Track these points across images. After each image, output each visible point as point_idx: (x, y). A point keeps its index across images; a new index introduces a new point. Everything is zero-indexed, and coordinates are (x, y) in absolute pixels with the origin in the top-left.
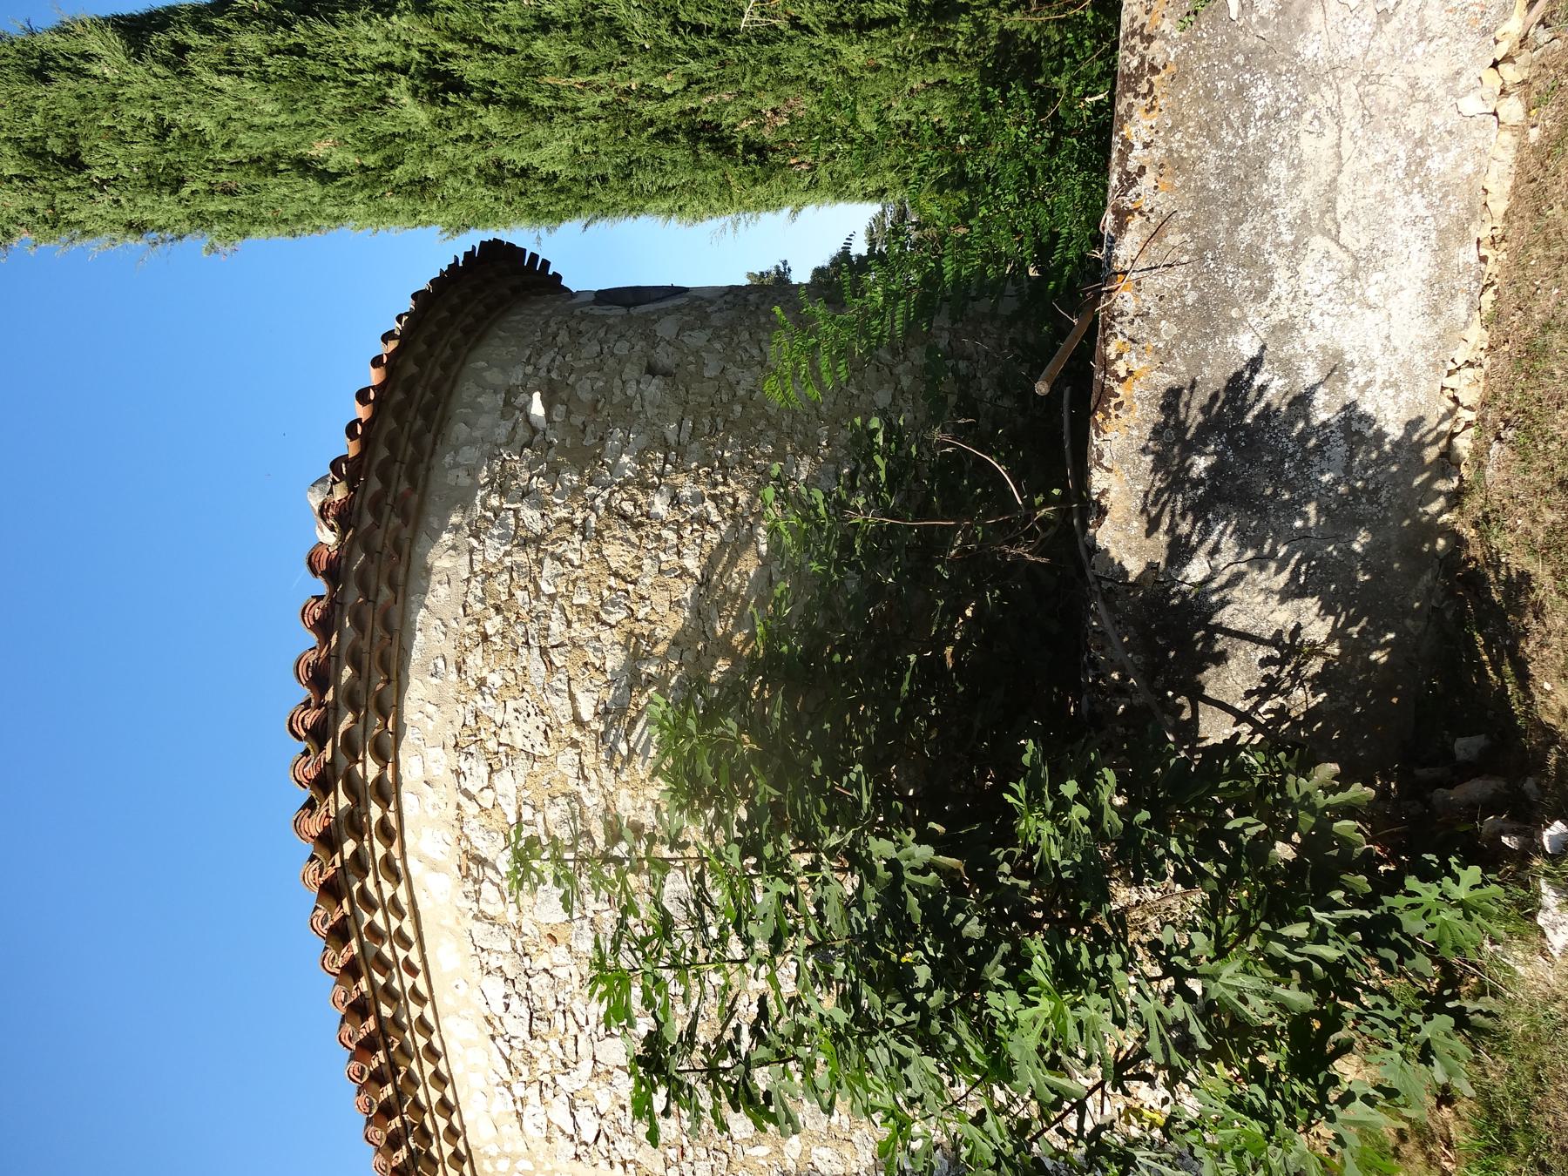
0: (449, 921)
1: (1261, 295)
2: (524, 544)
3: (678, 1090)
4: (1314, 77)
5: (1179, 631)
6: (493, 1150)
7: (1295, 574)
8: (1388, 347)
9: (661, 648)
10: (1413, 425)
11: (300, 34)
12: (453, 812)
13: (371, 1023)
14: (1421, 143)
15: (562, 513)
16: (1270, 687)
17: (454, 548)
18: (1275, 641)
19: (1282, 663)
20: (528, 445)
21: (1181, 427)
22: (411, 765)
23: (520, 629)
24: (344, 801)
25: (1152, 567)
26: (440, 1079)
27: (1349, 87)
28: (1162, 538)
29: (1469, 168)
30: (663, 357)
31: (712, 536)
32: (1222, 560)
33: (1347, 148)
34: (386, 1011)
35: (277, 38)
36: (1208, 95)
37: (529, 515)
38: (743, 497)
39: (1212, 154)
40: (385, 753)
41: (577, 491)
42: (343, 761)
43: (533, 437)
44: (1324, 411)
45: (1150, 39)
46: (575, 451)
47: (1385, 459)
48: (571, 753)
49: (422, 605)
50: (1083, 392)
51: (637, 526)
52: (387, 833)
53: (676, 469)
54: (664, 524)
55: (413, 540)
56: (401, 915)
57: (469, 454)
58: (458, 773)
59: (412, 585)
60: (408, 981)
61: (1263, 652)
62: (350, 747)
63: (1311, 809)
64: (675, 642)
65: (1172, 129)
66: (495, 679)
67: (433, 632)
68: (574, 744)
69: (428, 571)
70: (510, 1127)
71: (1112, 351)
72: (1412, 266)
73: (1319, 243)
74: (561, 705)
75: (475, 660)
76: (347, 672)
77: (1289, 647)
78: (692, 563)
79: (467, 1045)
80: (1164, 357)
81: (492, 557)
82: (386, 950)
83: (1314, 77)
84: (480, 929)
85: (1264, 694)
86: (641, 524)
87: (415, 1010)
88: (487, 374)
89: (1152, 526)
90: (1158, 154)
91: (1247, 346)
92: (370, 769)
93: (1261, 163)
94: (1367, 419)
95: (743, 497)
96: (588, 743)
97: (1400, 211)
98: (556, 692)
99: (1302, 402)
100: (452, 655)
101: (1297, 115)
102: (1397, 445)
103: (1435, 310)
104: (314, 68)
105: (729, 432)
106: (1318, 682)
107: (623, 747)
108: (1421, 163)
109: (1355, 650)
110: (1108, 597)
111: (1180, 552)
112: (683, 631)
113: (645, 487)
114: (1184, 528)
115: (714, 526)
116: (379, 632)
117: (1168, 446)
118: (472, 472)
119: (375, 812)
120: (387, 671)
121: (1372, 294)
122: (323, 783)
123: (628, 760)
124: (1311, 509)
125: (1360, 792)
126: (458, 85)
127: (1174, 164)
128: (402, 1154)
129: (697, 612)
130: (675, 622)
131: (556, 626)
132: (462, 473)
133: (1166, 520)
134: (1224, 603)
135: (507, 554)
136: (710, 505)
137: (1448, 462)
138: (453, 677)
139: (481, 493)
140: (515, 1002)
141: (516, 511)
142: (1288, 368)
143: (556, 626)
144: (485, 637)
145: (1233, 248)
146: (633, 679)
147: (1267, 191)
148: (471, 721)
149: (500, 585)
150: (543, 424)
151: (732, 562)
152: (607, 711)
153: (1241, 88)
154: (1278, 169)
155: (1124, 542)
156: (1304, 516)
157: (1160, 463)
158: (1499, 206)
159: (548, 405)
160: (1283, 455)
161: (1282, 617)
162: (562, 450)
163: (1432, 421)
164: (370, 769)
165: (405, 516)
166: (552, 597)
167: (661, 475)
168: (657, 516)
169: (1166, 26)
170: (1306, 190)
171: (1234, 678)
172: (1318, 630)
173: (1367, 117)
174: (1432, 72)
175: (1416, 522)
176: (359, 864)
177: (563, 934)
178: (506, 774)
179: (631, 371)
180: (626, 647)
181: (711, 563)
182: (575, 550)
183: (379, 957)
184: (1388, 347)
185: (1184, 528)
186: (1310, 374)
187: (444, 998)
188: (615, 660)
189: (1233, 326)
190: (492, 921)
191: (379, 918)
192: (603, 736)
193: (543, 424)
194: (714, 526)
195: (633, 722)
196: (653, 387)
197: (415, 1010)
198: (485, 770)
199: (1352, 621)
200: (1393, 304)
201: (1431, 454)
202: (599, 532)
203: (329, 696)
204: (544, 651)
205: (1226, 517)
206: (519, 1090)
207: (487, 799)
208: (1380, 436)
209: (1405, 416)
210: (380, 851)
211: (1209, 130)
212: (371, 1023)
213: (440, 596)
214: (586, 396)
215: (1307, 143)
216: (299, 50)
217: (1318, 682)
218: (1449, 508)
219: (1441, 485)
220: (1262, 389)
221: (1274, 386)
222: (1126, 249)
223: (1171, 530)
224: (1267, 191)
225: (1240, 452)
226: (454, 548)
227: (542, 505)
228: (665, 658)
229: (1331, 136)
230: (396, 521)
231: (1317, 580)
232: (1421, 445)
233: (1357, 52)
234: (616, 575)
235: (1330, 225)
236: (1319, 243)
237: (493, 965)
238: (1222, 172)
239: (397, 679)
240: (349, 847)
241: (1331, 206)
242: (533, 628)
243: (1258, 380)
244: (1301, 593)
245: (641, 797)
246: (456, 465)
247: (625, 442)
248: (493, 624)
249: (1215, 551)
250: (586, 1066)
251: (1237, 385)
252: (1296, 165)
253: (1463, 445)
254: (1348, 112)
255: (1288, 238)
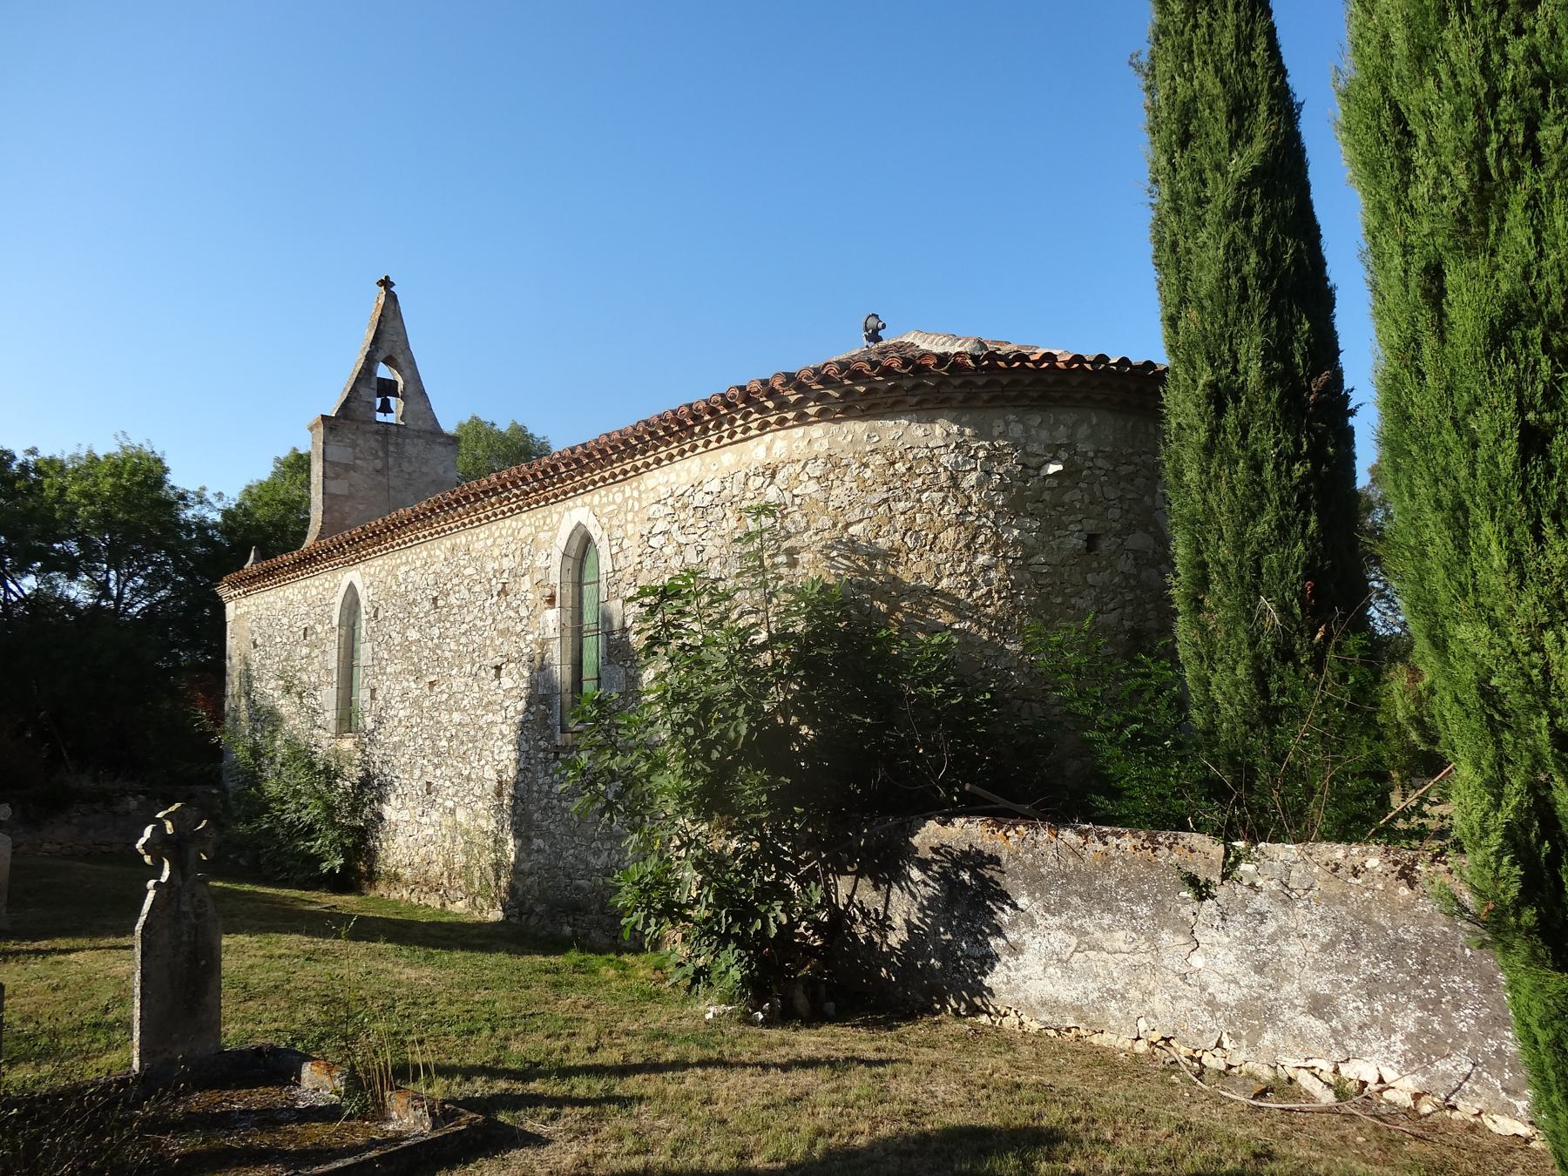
0: (744, 459)
1: (1047, 910)
2: (953, 478)
3: (652, 610)
4: (1152, 939)
5: (886, 864)
6: (642, 488)
7: (918, 928)
8: (1026, 978)
9: (891, 570)
10: (990, 991)
11: (1256, 296)
12: (796, 457)
13: (690, 423)
14: (1123, 997)
15: (975, 499)
16: (866, 915)
17: (948, 434)
18: (887, 918)
19: (876, 920)
20: (1025, 466)
21: (982, 866)
22: (817, 431)
23: (898, 484)
24: (792, 399)
25: (916, 850)
26: (671, 457)
27: (1148, 958)
28: (930, 855)
29: (1112, 1023)
30: (1104, 545)
31: (963, 594)
32: (921, 887)
33: (1120, 957)
34: (697, 429)
35: (1252, 281)
36: (1141, 880)
37: (972, 478)
38: (990, 610)
39: (1113, 882)
40: (823, 415)
41: (991, 505)
42: (814, 395)
43: (1031, 468)
44: (995, 943)
45: (1170, 848)
46: (1022, 497)
47: (974, 976)
48: (830, 524)
49: (911, 422)
50: (1000, 816)
51: (968, 547)
52: (782, 422)
53: (1009, 566)
54: (970, 563)
55: (951, 408)
56: (744, 432)
57: (1017, 430)
58: (816, 459)
59: (923, 414)
60: (713, 439)
61: (881, 909)
62: (821, 398)
63: (768, 911)
64: (895, 578)
65: (1124, 860)
66: (868, 473)
67: (898, 432)
68: (835, 525)
69: (932, 421)
70: (652, 497)
71: (1021, 828)
72: (1066, 992)
73: (1074, 941)
74: (855, 514)
75: (878, 459)
76: (862, 389)
77: (884, 925)
78: (944, 583)
79: (688, 471)
80: (1014, 856)
81: (943, 460)
82: (726, 426)
83: (1152, 939)
84: (742, 474)
85: (861, 910)
86: (969, 549)
87: (701, 443)
88: (1085, 426)
89: (935, 850)
90: (1112, 852)
91: (1022, 902)
92: (812, 410)
93: (1110, 910)
94: (992, 967)
95: (990, 610)
96: (835, 533)
97: (1091, 986)
98: (863, 511)
99: (998, 931)
100: (882, 445)
101: (1134, 929)
102: (981, 982)
103: (1044, 1004)
104: (1232, 309)
105: (1039, 596)
106: (869, 939)
107: (835, 553)
108: (1114, 997)
109: (885, 959)
110: (902, 826)
111: (924, 865)
112: (903, 582)
113: (995, 548)
114: (935, 868)
115: (970, 595)
116: (890, 401)
117: (972, 858)
118: (1003, 436)
119: (791, 415)
120: (869, 408)
121: (1051, 970)
122: (800, 387)
123: (828, 558)
124: (949, 937)
125: (774, 931)
126: (1220, 411)
127: (1107, 860)
128: (634, 442)
129: (914, 589)
130: (908, 578)
131: (901, 506)
132: (1001, 429)
133: (938, 858)
134: (902, 889)
135: (946, 469)
136: (984, 590)
137: (975, 1011)
138: (868, 448)
139: (987, 444)
140: (709, 498)
141: (975, 469)
142: (1014, 924)
143: (901, 506)
144: (893, 463)
145: (1069, 894)
146: (874, 554)
147: (1097, 913)
148: (844, 462)
149: (926, 468)
150: (1043, 474)
151: (946, 608)
152: (853, 542)
153: (1145, 898)
154: (1107, 919)
155: (930, 835)
156: (945, 933)
157: (965, 854)
158: (1095, 1040)
159: (1056, 474)
160: (973, 922)
161: (898, 921)
162: (1021, 490)
163: (993, 1002)
164: (812, 410)
165: (966, 400)
166: (919, 500)
167: (1005, 557)
168: (975, 558)
169: (1175, 856)
170: (1099, 934)
171: (868, 895)
172: (894, 939)
173: (1135, 968)
174: (1158, 1003)
175: (946, 993)
176: (763, 410)
177: (713, 550)
178: (816, 487)
179: (1090, 525)
180: (891, 549)
181: (944, 594)
182: (951, 510)
183: (721, 424)
184: (1026, 978)
185: (935, 868)
186: (1012, 936)
187: (708, 457)
188: (883, 543)
189: (1031, 894)
190: (746, 484)
191: (740, 422)
192: (840, 542)
193: (1043, 474)
194: (970, 595)
195: (848, 558)
196: (1076, 542)
197: (701, 443)
198: (818, 474)
199: (898, 957)
200: (1047, 981)
201: (978, 1001)
202: (962, 523)
203: (847, 382)
204: (886, 500)
205: (942, 890)
206: (670, 501)
207: (804, 477)
208: (985, 974)
209: (994, 987)
210: (772, 419)
211: (1124, 880)
212: (690, 423)
213: (918, 431)
214: (1066, 498)
215: (1120, 935)
216: (1244, 298)
217: (869, 939)
218: (953, 1010)
219: (963, 1005)
220: (1003, 910)
221: (1005, 916)
222: (1069, 835)
223: (934, 860)
224: (1097, 913)
225: (972, 897)
226: (948, 434)
227: (980, 484)
228: (885, 573)
229: (1125, 948)
230: (960, 397)
231: (917, 941)
232: (982, 996)
233: (1166, 962)
234: (935, 537)
235: (1083, 946)
236: (1074, 941)
237: (727, 484)
238: (1104, 888)
239: (864, 415)
240: (770, 404)
241: (1092, 948)
242: (899, 492)
243: (1007, 908)
244: (910, 931)
245: (812, 569)
246: (1007, 424)
247: (1029, 531)
248: (901, 467)
249: (926, 885)
250: (683, 540)
251: (1003, 896)
252: (1110, 930)
253: (984, 1019)
254: (1137, 957)
255: (1075, 924)
